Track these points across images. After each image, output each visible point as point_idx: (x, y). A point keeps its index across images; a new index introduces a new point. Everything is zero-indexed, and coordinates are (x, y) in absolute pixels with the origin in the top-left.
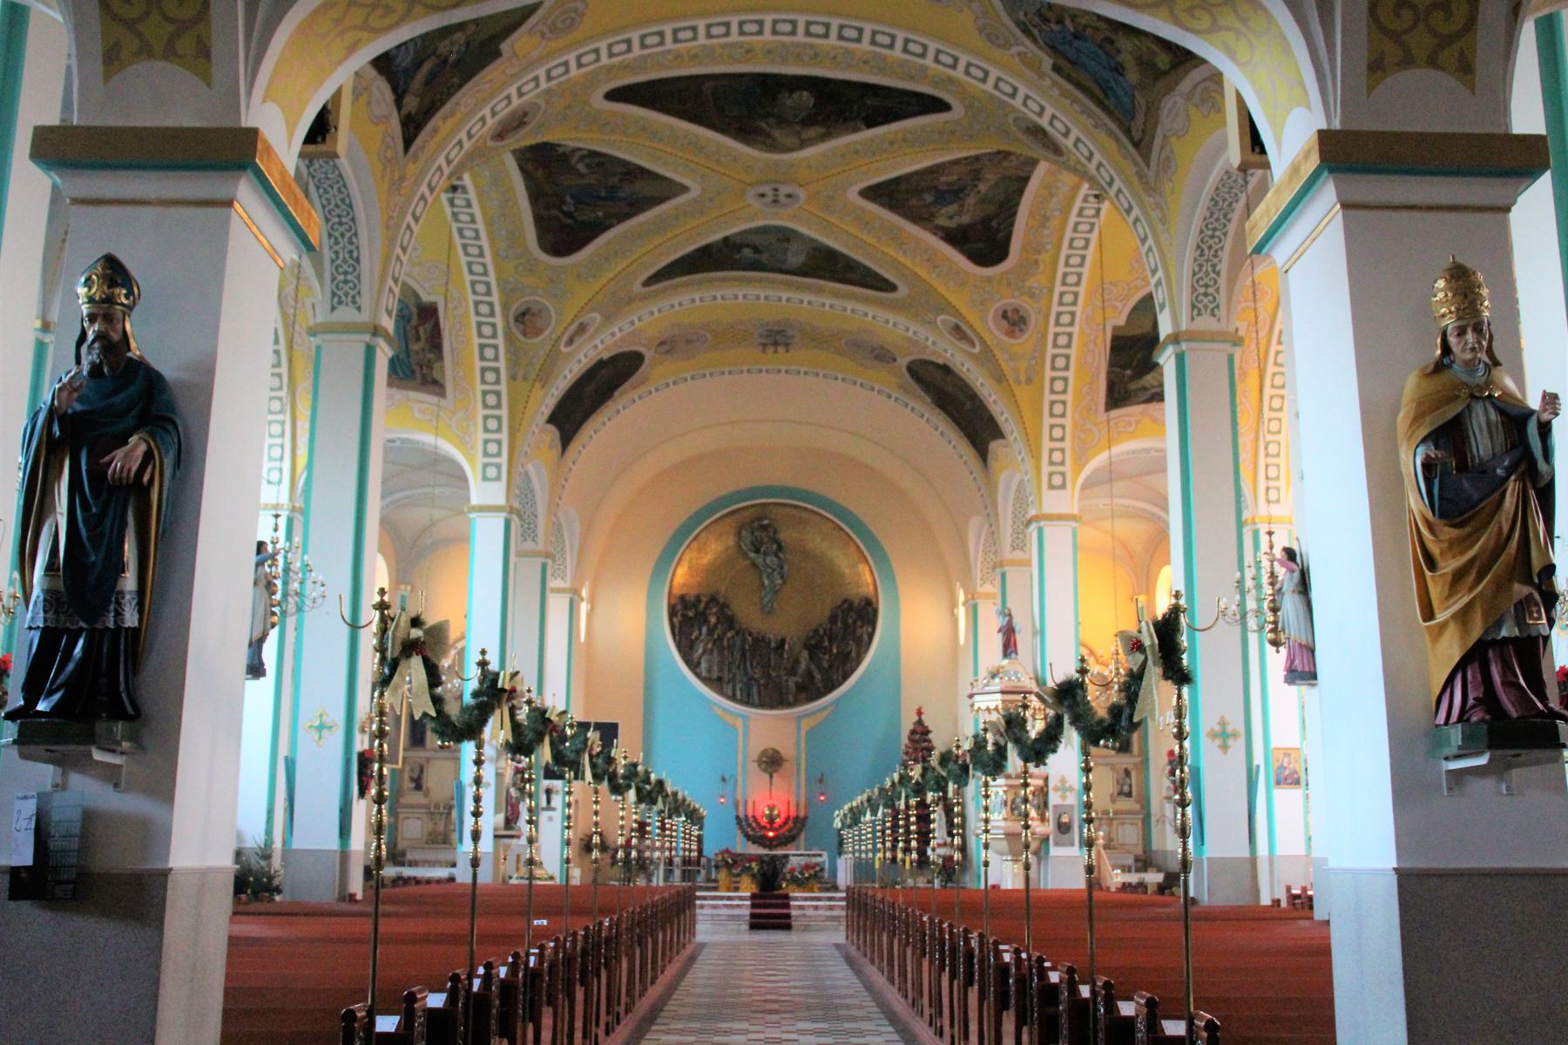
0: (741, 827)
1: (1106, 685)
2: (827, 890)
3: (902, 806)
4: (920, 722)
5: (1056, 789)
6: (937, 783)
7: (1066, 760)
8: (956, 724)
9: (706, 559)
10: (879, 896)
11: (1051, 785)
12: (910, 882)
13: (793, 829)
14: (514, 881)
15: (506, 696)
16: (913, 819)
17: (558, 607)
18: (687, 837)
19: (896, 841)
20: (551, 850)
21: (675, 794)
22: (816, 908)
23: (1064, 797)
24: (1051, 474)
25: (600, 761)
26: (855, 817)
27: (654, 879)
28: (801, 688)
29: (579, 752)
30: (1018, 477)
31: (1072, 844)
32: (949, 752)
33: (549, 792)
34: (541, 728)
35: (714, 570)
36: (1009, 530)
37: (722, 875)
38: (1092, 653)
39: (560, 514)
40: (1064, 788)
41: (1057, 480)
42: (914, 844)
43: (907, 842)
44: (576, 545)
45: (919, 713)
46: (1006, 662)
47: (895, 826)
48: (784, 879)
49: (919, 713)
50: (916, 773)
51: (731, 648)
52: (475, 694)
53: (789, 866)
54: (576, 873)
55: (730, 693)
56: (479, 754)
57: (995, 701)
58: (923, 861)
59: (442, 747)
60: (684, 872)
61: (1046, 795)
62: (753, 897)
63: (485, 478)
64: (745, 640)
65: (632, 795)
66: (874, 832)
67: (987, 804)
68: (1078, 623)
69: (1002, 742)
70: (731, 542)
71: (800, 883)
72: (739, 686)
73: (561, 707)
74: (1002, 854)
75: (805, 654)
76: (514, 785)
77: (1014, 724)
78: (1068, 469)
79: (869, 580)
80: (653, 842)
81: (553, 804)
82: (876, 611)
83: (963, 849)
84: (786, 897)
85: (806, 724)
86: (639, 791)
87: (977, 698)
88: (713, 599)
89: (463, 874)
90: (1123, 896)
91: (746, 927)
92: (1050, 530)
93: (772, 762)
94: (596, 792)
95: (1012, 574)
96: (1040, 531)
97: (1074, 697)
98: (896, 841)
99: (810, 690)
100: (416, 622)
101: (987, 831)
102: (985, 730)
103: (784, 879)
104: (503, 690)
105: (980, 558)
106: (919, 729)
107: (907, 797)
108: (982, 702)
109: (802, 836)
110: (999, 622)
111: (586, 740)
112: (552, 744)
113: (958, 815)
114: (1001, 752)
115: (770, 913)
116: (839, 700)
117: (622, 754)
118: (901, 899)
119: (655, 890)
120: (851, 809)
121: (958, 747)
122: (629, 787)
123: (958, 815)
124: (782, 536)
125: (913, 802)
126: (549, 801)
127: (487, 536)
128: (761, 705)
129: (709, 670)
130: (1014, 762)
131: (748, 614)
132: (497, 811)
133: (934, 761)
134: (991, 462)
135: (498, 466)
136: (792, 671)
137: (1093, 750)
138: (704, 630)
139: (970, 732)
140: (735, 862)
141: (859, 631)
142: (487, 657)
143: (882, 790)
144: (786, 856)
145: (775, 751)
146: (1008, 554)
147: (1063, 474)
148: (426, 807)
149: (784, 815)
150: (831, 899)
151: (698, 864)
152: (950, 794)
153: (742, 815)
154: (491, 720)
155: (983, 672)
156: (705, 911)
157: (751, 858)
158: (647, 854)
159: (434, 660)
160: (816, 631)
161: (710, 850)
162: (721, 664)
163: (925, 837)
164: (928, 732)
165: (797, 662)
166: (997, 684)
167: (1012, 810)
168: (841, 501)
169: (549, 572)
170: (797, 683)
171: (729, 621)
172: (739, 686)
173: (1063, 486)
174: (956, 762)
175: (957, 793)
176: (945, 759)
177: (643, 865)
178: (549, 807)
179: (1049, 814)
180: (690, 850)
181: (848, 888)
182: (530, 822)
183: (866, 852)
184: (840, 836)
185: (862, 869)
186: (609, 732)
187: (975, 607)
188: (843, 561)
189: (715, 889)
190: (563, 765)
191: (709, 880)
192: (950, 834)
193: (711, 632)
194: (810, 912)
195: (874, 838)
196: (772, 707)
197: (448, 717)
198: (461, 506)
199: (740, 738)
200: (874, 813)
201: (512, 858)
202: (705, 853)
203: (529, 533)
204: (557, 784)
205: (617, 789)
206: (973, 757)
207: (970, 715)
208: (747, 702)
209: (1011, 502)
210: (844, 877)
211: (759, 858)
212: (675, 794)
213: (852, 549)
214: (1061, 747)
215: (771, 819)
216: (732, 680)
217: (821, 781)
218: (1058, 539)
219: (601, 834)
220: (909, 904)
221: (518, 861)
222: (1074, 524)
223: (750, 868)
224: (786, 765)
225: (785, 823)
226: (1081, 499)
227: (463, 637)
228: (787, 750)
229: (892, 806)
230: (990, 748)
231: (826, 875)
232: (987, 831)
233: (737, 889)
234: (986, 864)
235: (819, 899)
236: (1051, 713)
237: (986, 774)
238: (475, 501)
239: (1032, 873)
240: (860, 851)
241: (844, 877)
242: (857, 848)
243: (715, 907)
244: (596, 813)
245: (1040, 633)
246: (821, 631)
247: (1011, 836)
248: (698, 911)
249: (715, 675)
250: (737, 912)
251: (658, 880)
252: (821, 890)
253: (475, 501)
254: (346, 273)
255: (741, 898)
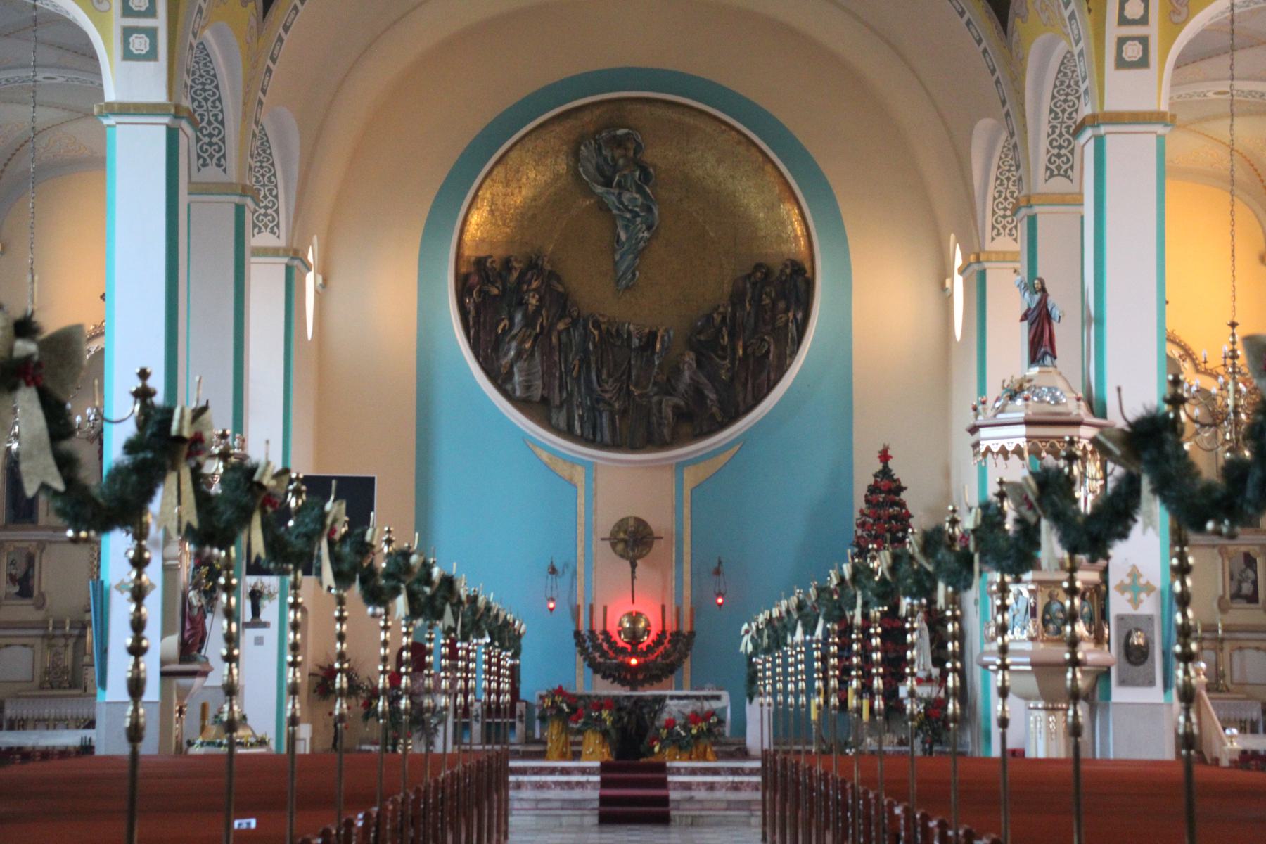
0: (583, 651)
1: (1215, 419)
2: (730, 756)
3: (858, 620)
4: (885, 473)
5: (1122, 588)
6: (918, 582)
7: (1144, 549)
8: (947, 474)
9: (520, 197)
10: (819, 769)
11: (1113, 581)
12: (870, 743)
13: (671, 653)
14: (196, 750)
15: (185, 448)
16: (876, 642)
17: (265, 283)
18: (494, 669)
19: (845, 671)
20: (259, 682)
21: (473, 599)
22: (711, 787)
23: (1135, 602)
24: (1121, 41)
25: (346, 549)
26: (777, 634)
27: (439, 742)
28: (682, 415)
29: (311, 538)
30: (1061, 48)
31: (1151, 683)
32: (939, 530)
33: (256, 596)
34: (245, 499)
35: (529, 218)
36: (1044, 143)
37: (553, 732)
38: (1188, 354)
39: (265, 121)
40: (1135, 586)
41: (1132, 51)
42: (878, 683)
43: (867, 678)
44: (295, 168)
45: (885, 456)
46: (1035, 370)
47: (845, 647)
48: (657, 738)
49: (885, 456)
50: (880, 563)
51: (564, 348)
52: (130, 447)
53: (665, 716)
54: (304, 731)
55: (563, 425)
56: (140, 550)
57: (1016, 436)
58: (894, 707)
59: (75, 540)
60: (487, 728)
61: (1104, 597)
62: (605, 768)
63: (128, 55)
64: (586, 336)
65: (401, 604)
66: (809, 661)
67: (1002, 623)
68: (1163, 302)
69: (1031, 518)
70: (562, 168)
71: (685, 746)
72: (578, 413)
73: (277, 465)
74: (1027, 698)
75: (690, 357)
76: (196, 586)
77: (1052, 489)
78: (1153, 30)
79: (799, 230)
80: (438, 681)
81: (264, 616)
82: (810, 285)
83: (962, 694)
84: (662, 768)
85: (690, 478)
86: (412, 598)
87: (984, 432)
88: (533, 265)
89: (109, 741)
90: (1242, 776)
91: (592, 820)
92: (1119, 143)
93: (634, 540)
94: (341, 601)
95: (1047, 218)
96: (1099, 142)
97: (1160, 444)
98: (845, 671)
99: (698, 419)
100: (24, 328)
101: (1004, 667)
102: (1002, 496)
103: (657, 738)
104: (180, 439)
105: (991, 192)
106: (884, 483)
107: (866, 605)
108: (991, 438)
109: (687, 664)
110: (1019, 302)
111: (324, 515)
112: (265, 527)
113: (954, 637)
114: (1029, 534)
115: (634, 794)
116: (743, 439)
117: (386, 531)
118: (856, 776)
119: (440, 760)
120: (770, 621)
121: (954, 522)
122: (396, 592)
123: (954, 637)
124: (652, 155)
125: (875, 612)
126: (256, 611)
127: (136, 161)
128: (615, 446)
129: (528, 387)
130: (1051, 547)
131: (593, 291)
132: (166, 632)
133: (912, 544)
134: (1015, 22)
135: (152, 33)
136: (668, 389)
137: (1193, 537)
138: (518, 317)
139: (973, 499)
140: (574, 709)
141: (781, 319)
142: (151, 383)
143: (822, 590)
144: (660, 700)
145: (640, 522)
146: (1041, 183)
147: (1144, 41)
148: (43, 625)
149: (655, 629)
150: (735, 772)
151: (513, 715)
152: (941, 602)
153: (584, 629)
154: (160, 492)
155: (994, 390)
156: (526, 794)
157: (601, 703)
158: (427, 701)
159: (58, 393)
160: (709, 318)
161: (531, 689)
162: (547, 374)
163: (896, 668)
164: (901, 489)
165: (678, 371)
166: (1018, 410)
167: (1045, 623)
168: (753, 96)
169: (249, 218)
170: (676, 408)
171: (560, 302)
172: (578, 413)
173: (1143, 63)
174: (950, 547)
175: (954, 600)
176: (934, 540)
177: (420, 720)
178: (256, 622)
179: (1111, 631)
180: (499, 692)
181: (765, 756)
182: (230, 658)
183: (796, 694)
184: (751, 664)
185: (787, 722)
186: (359, 493)
187: (982, 275)
188: (752, 197)
189: (541, 755)
190: (287, 555)
191: (529, 740)
192: (938, 661)
193: (529, 322)
194: (701, 794)
195: (809, 671)
196: (633, 448)
197: (85, 489)
198: (87, 103)
199: (581, 501)
200: (810, 629)
201: (193, 710)
202: (523, 695)
203: (211, 152)
204: (271, 582)
205: (376, 596)
206: (979, 541)
207: (980, 467)
208: (591, 439)
209: (1048, 91)
210: (757, 735)
211: (613, 703)
212: (473, 599)
213: (771, 177)
214: (1136, 531)
215: (634, 636)
216: (567, 403)
217: (717, 572)
218: (1130, 155)
219: (348, 673)
220: (869, 782)
221: (204, 716)
222: (1160, 129)
223: (599, 719)
224: (657, 546)
225: (658, 642)
226: (1174, 85)
227: (99, 333)
228: (659, 521)
229: (841, 619)
230: (1009, 525)
231: (727, 730)
232: (1004, 667)
233: (577, 756)
234: (1004, 723)
235: (715, 772)
236: (1117, 471)
237: (1003, 571)
238: (111, 95)
239: (1085, 736)
240: (785, 693)
241: (757, 735)
242: (776, 692)
243: (540, 786)
244: (341, 637)
245: (1095, 320)
246: (717, 318)
247: (1041, 668)
248: (512, 793)
249: (537, 394)
250: (577, 794)
251: (443, 743)
252: (719, 756)
253: (111, 95)
254: (211, 144)
255: (584, 771)
